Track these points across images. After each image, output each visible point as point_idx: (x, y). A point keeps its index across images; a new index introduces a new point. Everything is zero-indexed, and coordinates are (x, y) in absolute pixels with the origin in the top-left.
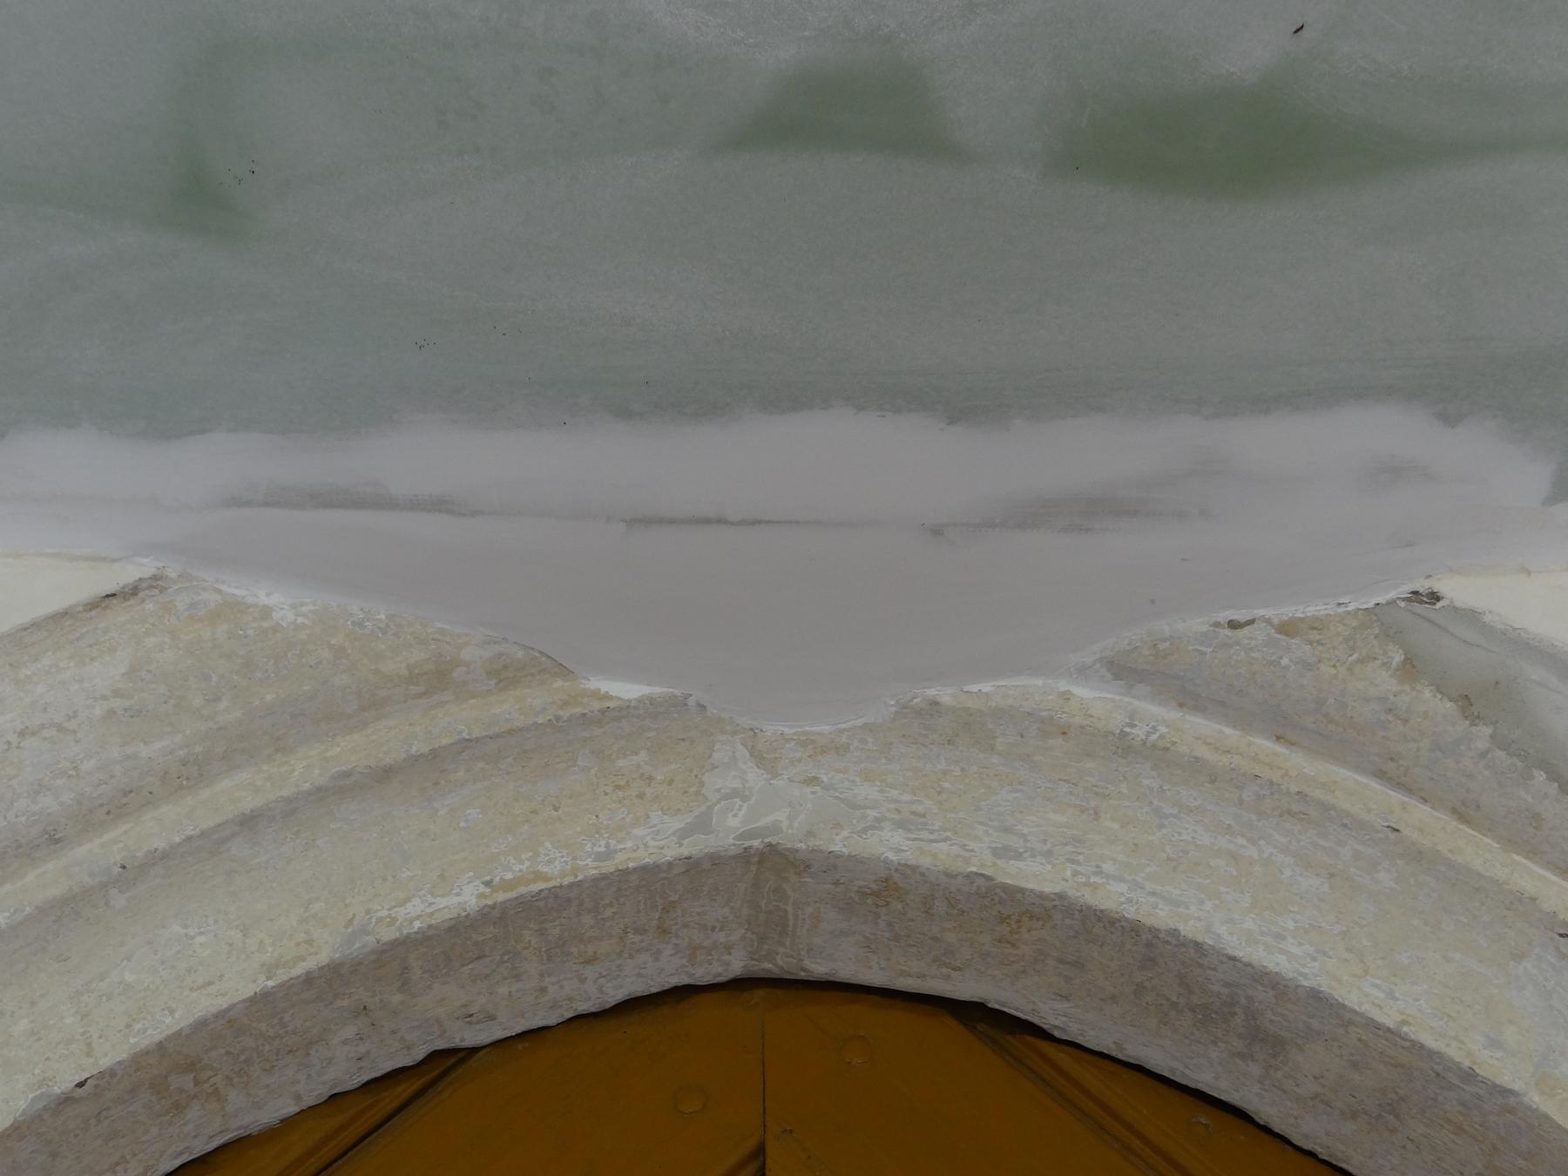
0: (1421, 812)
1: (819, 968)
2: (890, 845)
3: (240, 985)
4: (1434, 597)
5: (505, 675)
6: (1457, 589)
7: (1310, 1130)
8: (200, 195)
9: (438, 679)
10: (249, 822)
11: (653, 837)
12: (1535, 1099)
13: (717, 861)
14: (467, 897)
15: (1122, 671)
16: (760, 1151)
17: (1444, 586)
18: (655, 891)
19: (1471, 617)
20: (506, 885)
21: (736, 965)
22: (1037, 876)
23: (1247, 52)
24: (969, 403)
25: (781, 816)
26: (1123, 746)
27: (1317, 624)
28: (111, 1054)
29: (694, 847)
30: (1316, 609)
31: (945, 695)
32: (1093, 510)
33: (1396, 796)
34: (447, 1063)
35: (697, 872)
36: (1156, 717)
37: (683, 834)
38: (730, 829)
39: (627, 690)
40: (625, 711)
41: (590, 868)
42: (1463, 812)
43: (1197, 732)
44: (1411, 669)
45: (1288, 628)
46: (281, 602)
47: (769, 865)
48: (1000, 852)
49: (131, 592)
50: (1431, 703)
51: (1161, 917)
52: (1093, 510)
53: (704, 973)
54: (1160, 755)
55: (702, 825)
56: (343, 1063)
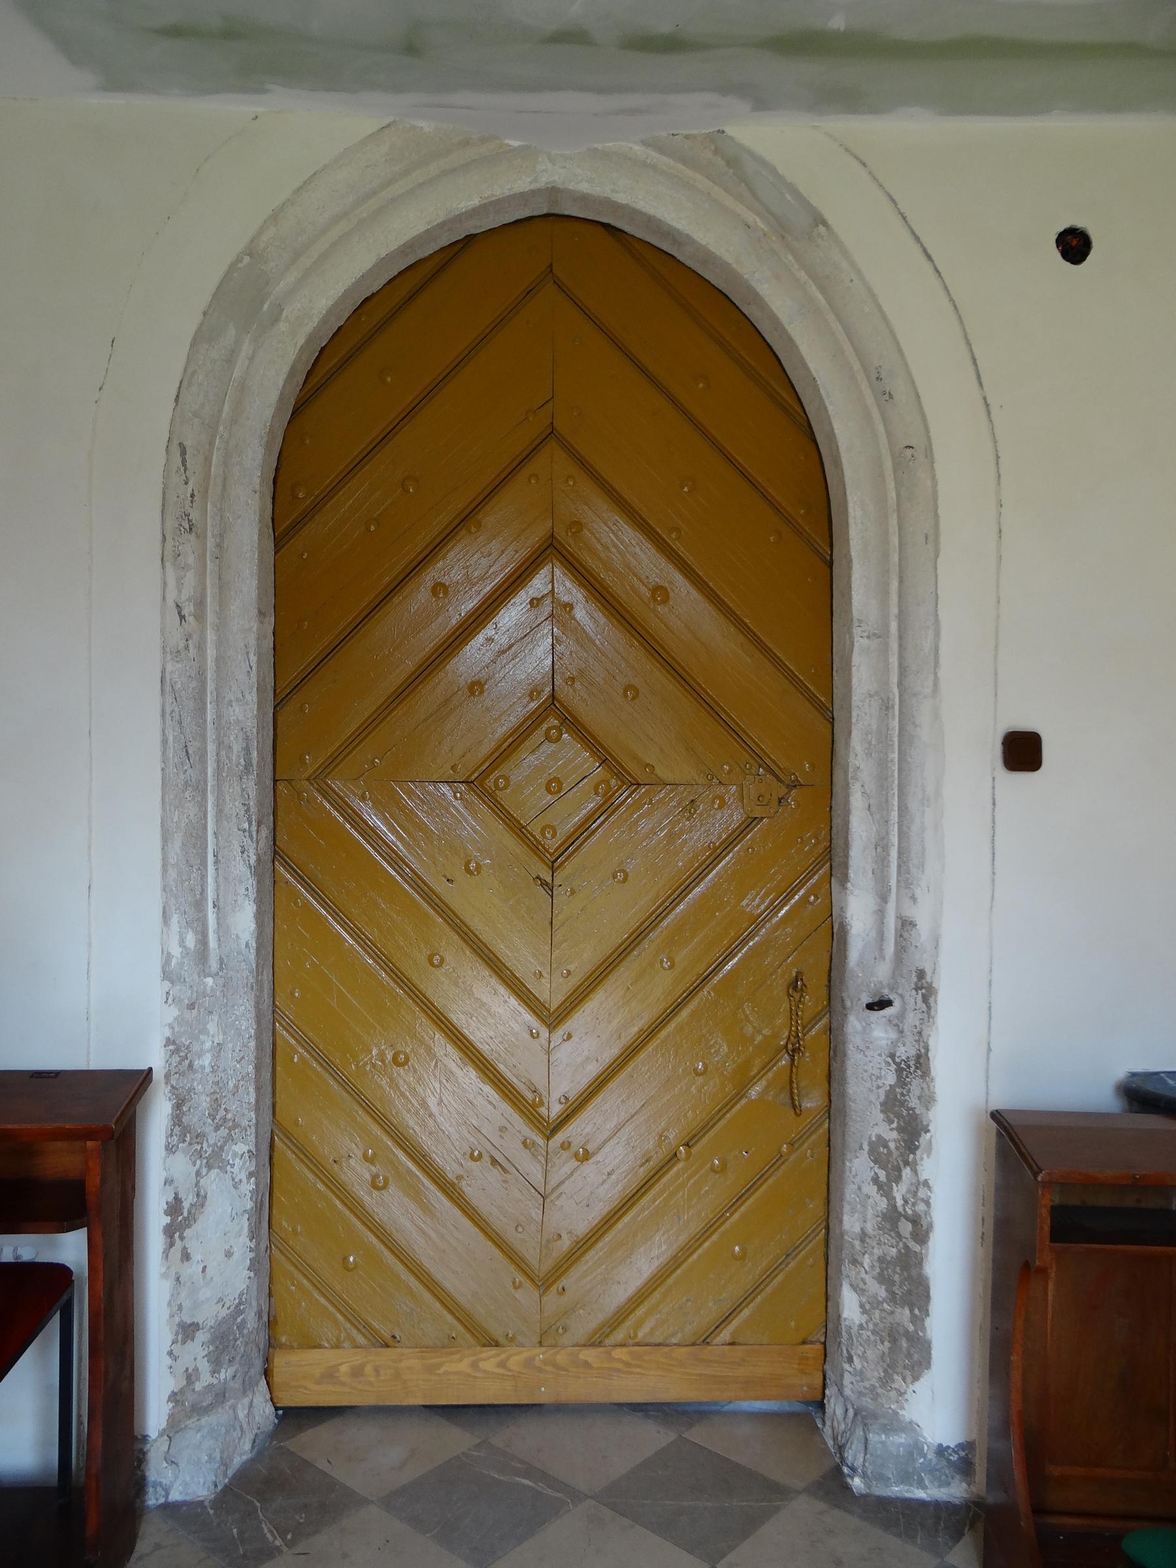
0: (717, 189)
1: (566, 213)
2: (584, 187)
3: (422, 228)
4: (723, 132)
5: (483, 140)
6: (730, 130)
7: (688, 263)
8: (411, 49)
9: (466, 143)
10: (421, 185)
11: (523, 184)
12: (734, 266)
13: (539, 190)
14: (475, 202)
15: (645, 143)
16: (551, 265)
17: (726, 129)
18: (524, 197)
19: (732, 138)
20: (486, 198)
21: (545, 212)
22: (622, 198)
23: (665, 28)
24: (600, 90)
25: (556, 178)
26: (644, 164)
27: (695, 137)
28: (393, 247)
29: (534, 186)
30: (694, 132)
31: (599, 146)
32: (633, 112)
33: (711, 184)
34: (470, 239)
35: (534, 193)
36: (654, 156)
37: (531, 183)
38: (543, 181)
39: (515, 143)
40: (515, 149)
41: (507, 193)
42: (726, 190)
43: (664, 161)
44: (716, 152)
45: (687, 137)
46: (426, 126)
47: (553, 192)
48: (613, 191)
49: (388, 126)
50: (720, 162)
51: (651, 211)
52: (633, 112)
53: (536, 213)
54: (654, 167)
55: (535, 180)
56: (445, 241)
